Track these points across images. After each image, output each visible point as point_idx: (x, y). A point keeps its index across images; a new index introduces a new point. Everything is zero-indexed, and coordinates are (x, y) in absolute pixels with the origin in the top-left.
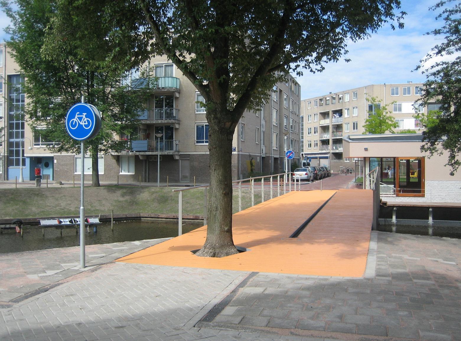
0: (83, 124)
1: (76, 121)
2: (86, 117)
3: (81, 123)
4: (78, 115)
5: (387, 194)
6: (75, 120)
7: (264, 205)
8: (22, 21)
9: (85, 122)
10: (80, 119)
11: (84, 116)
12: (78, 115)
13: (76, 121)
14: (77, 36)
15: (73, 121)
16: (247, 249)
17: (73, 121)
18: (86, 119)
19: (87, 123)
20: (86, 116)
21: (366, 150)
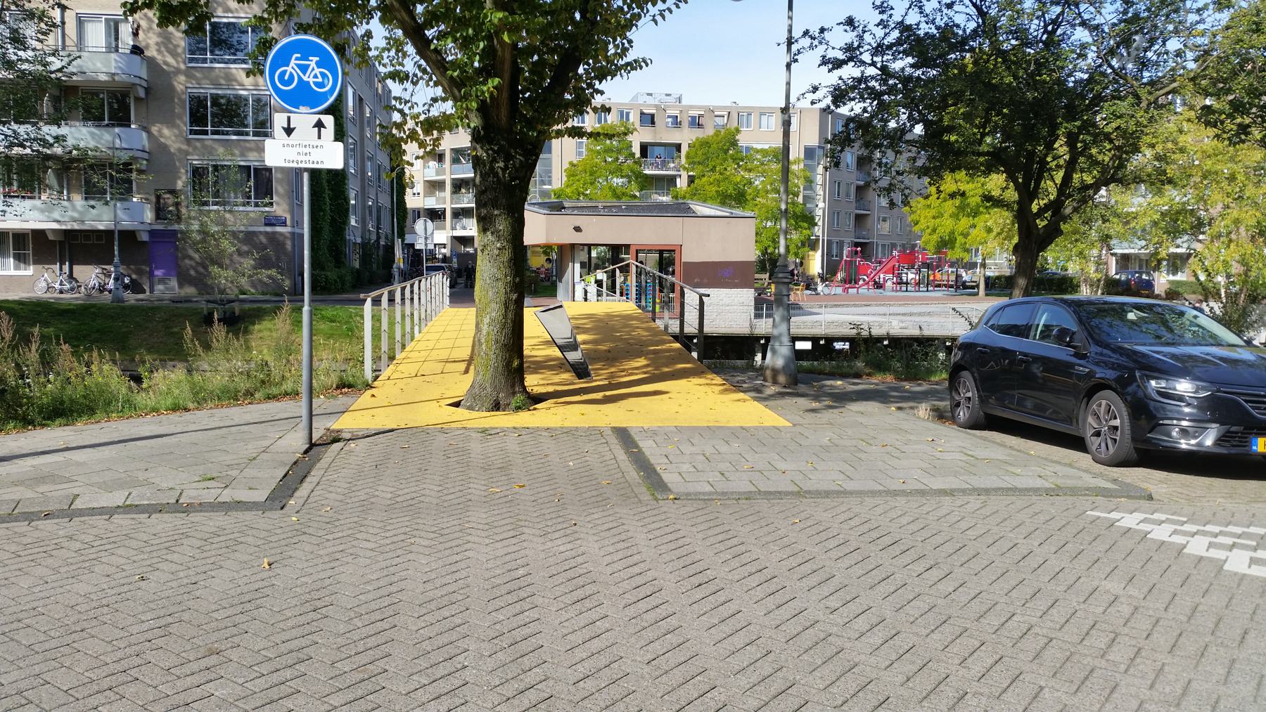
0: (311, 80)
1: (291, 74)
2: (319, 65)
3: (305, 78)
4: (297, 59)
5: (920, 314)
6: (289, 69)
7: (820, 209)
8: (164, 367)
9: (315, 76)
10: (304, 69)
11: (313, 64)
12: (297, 59)
13: (291, 74)
14: (455, 260)
15: (284, 73)
16: (340, 145)
17: (284, 73)
18: (317, 71)
19: (320, 80)
20: (317, 63)
21: (578, 229)
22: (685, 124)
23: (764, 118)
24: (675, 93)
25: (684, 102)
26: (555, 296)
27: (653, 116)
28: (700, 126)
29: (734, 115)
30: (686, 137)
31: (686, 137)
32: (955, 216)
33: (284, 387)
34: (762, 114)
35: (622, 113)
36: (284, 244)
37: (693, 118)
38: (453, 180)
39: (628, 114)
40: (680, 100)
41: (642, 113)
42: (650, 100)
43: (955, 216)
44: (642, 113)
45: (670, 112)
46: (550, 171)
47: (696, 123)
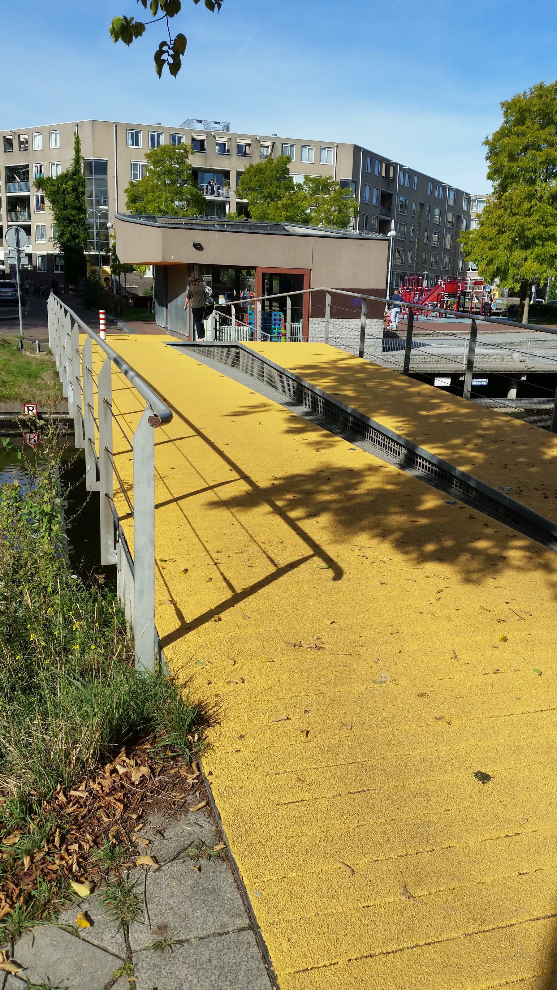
21: (198, 247)
22: (234, 152)
23: (305, 151)
24: (224, 121)
25: (232, 130)
26: (154, 320)
27: (202, 142)
28: (246, 155)
29: (278, 146)
30: (234, 165)
31: (234, 165)
32: (510, 248)
33: (99, 789)
34: (303, 147)
35: (174, 137)
36: (459, 246)
37: (240, 146)
38: (9, 198)
39: (180, 139)
40: (227, 127)
41: (193, 140)
42: (199, 127)
43: (510, 248)
44: (193, 140)
45: (219, 140)
46: (106, 192)
47: (242, 151)
